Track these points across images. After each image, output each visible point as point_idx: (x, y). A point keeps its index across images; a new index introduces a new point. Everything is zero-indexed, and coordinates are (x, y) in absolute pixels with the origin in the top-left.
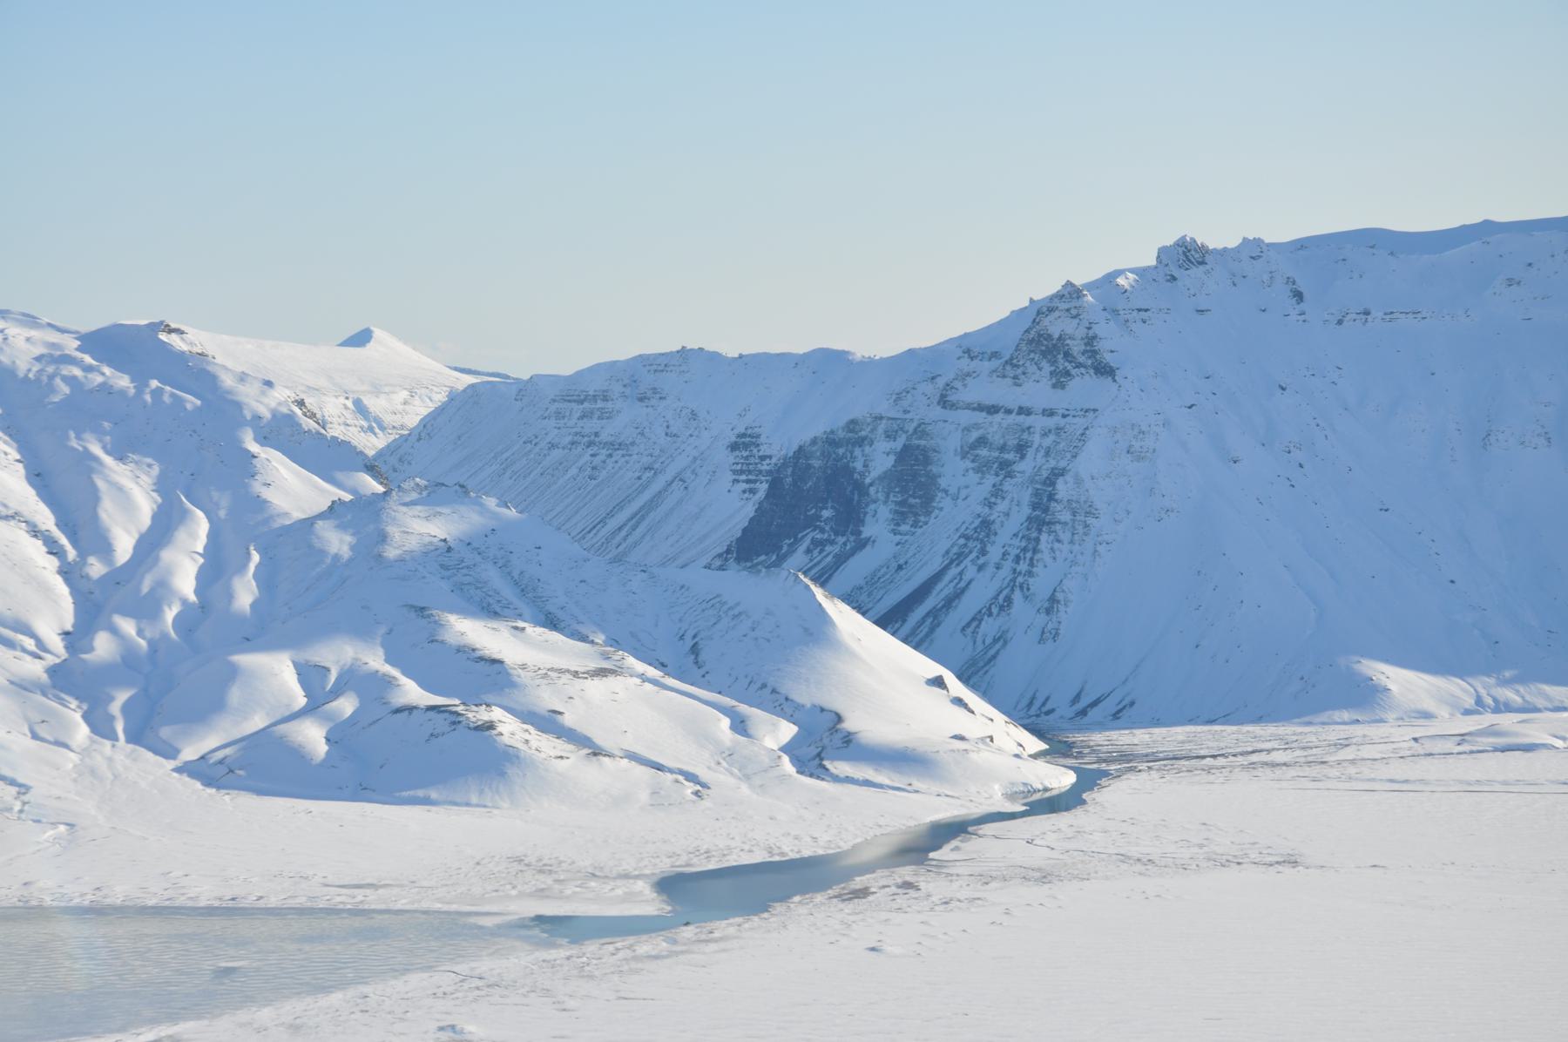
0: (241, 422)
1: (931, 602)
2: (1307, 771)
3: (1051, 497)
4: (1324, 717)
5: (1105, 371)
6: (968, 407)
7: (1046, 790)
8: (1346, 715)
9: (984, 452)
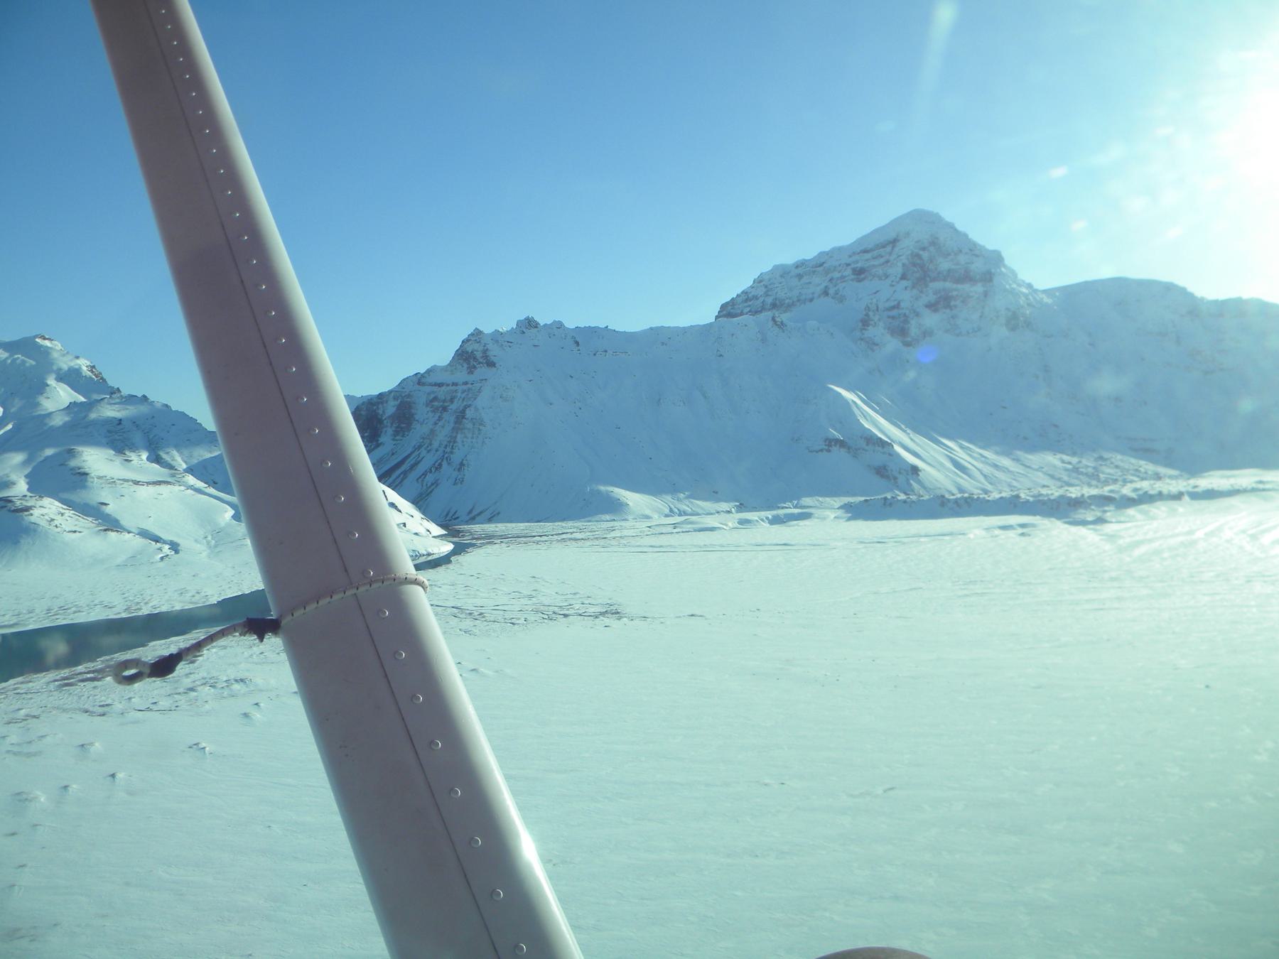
0: (50, 371)
1: (403, 468)
2: (597, 542)
3: (463, 417)
4: (597, 518)
5: (491, 364)
6: (431, 385)
7: (429, 554)
8: (608, 517)
9: (436, 404)
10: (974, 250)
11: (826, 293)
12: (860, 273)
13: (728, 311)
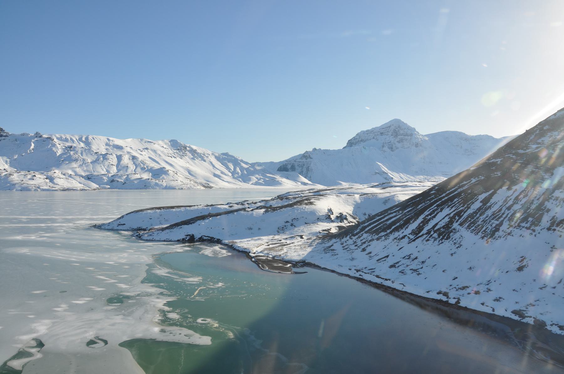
10: (409, 128)
11: (374, 138)
12: (382, 134)
13: (351, 143)
